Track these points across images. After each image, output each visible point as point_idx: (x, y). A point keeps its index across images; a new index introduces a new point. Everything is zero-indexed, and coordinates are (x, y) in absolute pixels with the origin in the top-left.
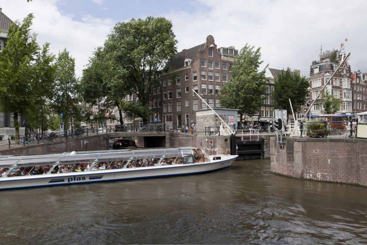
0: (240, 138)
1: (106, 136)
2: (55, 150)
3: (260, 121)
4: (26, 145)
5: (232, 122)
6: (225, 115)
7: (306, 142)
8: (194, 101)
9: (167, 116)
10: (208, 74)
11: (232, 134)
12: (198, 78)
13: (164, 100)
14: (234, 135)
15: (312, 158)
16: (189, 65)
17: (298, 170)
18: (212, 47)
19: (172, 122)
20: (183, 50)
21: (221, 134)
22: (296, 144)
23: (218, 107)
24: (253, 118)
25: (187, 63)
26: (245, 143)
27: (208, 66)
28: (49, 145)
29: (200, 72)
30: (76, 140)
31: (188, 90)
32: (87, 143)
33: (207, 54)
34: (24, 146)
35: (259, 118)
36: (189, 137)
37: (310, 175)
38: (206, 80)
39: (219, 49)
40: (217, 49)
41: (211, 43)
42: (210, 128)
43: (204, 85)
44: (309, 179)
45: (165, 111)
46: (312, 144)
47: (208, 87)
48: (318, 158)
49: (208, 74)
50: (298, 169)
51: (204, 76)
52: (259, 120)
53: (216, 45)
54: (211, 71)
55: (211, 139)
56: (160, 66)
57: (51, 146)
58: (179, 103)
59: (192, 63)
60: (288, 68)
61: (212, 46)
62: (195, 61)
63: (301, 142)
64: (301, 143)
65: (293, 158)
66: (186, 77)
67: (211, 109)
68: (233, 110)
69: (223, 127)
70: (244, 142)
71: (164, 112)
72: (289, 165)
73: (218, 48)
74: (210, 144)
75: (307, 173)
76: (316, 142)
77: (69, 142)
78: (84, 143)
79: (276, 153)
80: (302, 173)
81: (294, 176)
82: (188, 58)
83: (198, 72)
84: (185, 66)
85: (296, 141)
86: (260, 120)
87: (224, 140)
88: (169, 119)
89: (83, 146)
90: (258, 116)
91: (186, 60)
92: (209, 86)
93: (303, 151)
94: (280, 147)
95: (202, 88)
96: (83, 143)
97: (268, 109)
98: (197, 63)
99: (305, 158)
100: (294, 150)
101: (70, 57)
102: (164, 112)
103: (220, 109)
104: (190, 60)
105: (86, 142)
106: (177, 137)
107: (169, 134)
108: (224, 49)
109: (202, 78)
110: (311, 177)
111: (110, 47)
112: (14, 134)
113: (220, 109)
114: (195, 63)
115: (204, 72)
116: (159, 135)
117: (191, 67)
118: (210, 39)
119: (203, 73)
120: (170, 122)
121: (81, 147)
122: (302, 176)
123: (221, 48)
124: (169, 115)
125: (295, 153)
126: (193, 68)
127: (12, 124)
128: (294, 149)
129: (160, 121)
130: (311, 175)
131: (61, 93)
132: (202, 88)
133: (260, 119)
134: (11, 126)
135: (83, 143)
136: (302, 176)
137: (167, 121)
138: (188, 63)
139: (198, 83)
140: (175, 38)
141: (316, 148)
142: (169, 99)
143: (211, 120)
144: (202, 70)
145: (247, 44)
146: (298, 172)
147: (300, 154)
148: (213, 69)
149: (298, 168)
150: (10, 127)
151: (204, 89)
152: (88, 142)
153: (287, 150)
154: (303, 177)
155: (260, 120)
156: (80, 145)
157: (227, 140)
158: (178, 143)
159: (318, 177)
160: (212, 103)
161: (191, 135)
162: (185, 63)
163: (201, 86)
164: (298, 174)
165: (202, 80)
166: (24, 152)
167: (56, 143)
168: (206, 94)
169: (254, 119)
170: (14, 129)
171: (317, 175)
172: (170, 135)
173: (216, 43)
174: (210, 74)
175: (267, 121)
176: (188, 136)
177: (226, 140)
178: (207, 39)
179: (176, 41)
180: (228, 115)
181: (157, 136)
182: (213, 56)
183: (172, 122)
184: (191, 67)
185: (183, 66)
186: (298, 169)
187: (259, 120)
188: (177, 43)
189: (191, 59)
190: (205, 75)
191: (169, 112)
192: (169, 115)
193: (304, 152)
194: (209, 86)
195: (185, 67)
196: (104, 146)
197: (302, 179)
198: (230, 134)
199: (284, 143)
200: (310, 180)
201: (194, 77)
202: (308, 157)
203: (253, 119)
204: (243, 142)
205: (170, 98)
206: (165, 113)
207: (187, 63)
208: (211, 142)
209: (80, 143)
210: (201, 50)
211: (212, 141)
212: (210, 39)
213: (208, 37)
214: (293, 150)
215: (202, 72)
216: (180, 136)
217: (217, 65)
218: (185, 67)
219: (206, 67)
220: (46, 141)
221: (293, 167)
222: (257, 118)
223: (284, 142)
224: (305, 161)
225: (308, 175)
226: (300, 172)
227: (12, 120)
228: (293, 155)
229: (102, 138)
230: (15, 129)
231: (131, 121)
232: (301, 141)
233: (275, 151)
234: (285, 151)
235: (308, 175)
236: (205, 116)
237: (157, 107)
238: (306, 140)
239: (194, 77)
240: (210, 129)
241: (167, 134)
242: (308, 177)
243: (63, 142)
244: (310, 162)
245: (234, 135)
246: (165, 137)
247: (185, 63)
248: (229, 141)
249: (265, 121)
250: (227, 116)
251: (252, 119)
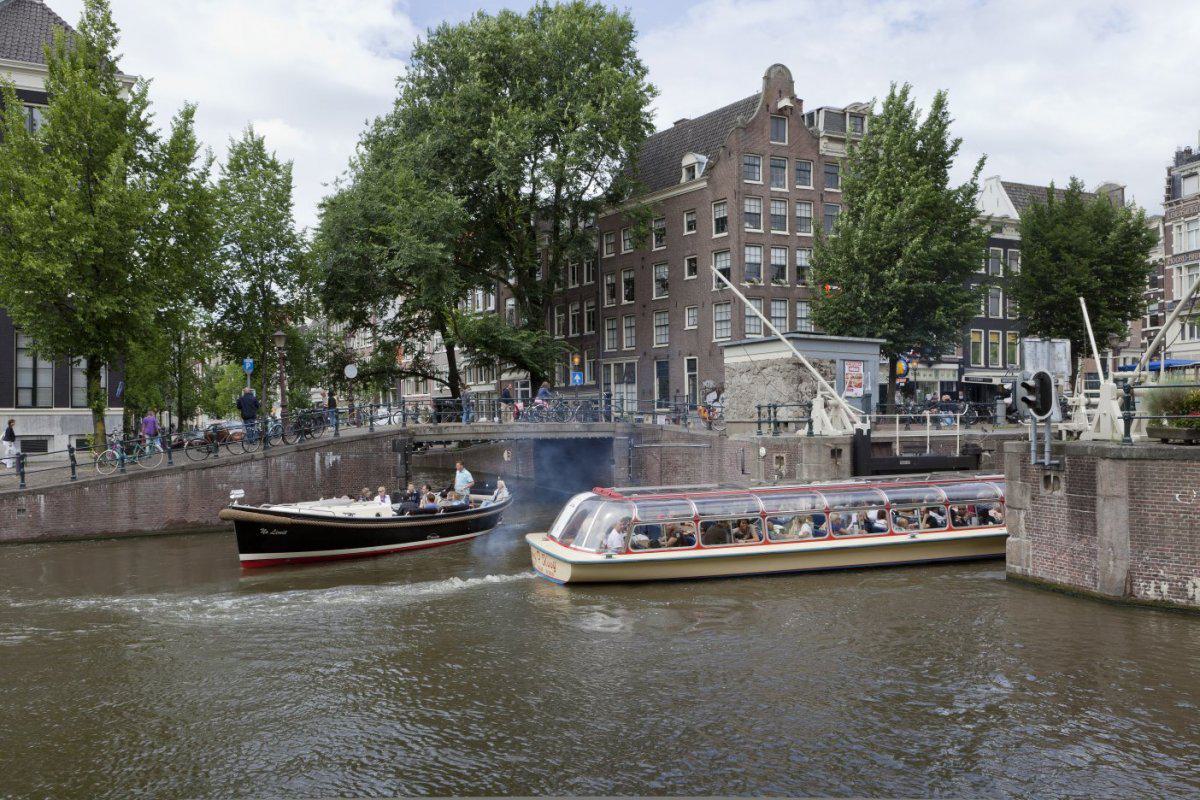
0: (887, 445)
1: (400, 437)
2: (225, 485)
3: (963, 381)
4: (130, 470)
5: (859, 386)
6: (833, 362)
7: (1145, 459)
8: (718, 307)
9: (619, 366)
10: (767, 209)
11: (859, 431)
12: (732, 224)
13: (606, 306)
14: (865, 433)
15: (1169, 522)
16: (698, 175)
17: (1111, 569)
18: (785, 107)
19: (634, 388)
20: (675, 124)
21: (816, 431)
22: (1104, 467)
23: (804, 330)
24: (937, 371)
25: (691, 169)
26: (907, 463)
27: (773, 177)
28: (204, 469)
29: (740, 204)
30: (299, 450)
31: (693, 270)
32: (335, 463)
33: (768, 133)
34: (123, 471)
35: (961, 372)
36: (697, 442)
37: (1159, 588)
38: (761, 231)
39: (811, 116)
40: (803, 116)
41: (780, 92)
42: (775, 407)
43: (753, 249)
44: (1155, 601)
45: (608, 346)
46: (1170, 467)
47: (793, 259)
48: (1192, 522)
49: (767, 209)
50: (1111, 563)
51: (754, 218)
52: (960, 378)
53: (800, 102)
54: (780, 198)
55: (778, 448)
56: (594, 182)
57: (212, 471)
58: (663, 316)
59: (710, 168)
60: (1073, 179)
61: (785, 102)
62: (722, 163)
63: (1125, 459)
64: (1125, 465)
65: (1094, 521)
66: (689, 223)
67: (779, 340)
68: (855, 342)
69: (826, 406)
70: (905, 459)
71: (607, 350)
72: (1078, 546)
73: (806, 109)
74: (776, 466)
75: (1148, 579)
76: (1185, 460)
77: (273, 460)
78: (327, 463)
79: (1027, 500)
80: (1130, 580)
81: (1097, 590)
82: (696, 152)
83: (731, 200)
84: (684, 180)
85: (1105, 458)
86: (963, 378)
87: (829, 452)
88: (627, 376)
89: (323, 474)
90: (959, 362)
91: (689, 159)
92: (773, 252)
93: (1132, 494)
94: (1041, 479)
95: (747, 260)
96: (322, 462)
97: (978, 335)
98: (728, 169)
99: (1142, 522)
100: (1100, 491)
101: (270, 157)
102: (607, 350)
103: (812, 336)
104: (704, 159)
105: (331, 458)
106: (656, 441)
107: (626, 431)
108: (829, 113)
109: (747, 225)
110: (1165, 593)
111: (414, 121)
112: (88, 430)
113: (812, 336)
114: (720, 171)
115: (753, 202)
116: (590, 435)
117: (704, 184)
118: (779, 79)
119: (751, 206)
120: (629, 387)
121: (313, 475)
122: (1128, 591)
123: (818, 110)
124: (625, 361)
125: (1100, 502)
126: (715, 190)
127: (80, 396)
128: (1099, 486)
129: (593, 383)
130: (1165, 587)
131: (243, 287)
132: (747, 260)
133: (967, 375)
134: (21, 402)
135: (322, 462)
136: (1128, 591)
137: (619, 382)
138: (696, 169)
139: (732, 244)
140: (647, 80)
141: (1185, 483)
142: (625, 302)
143: (780, 380)
144: (748, 193)
145: (894, 87)
146: (1114, 575)
147: (1123, 507)
148: (786, 190)
149: (1114, 560)
150: (16, 407)
151: (755, 264)
152: (339, 457)
153: (1068, 491)
154: (1131, 594)
155: (967, 379)
156: (313, 468)
157: (840, 451)
158: (658, 465)
159: (1190, 594)
160: (783, 315)
161: (705, 433)
162: (684, 170)
163: (742, 256)
164: (1112, 580)
165: (747, 230)
166: (122, 492)
167: (228, 464)
168: (762, 284)
169: (940, 373)
170: (89, 412)
171: (1189, 586)
172: (630, 435)
173: (799, 92)
174: (778, 209)
175: (991, 380)
176: (692, 438)
177: (836, 453)
178: (767, 78)
179: (650, 88)
180: (844, 360)
181: (582, 436)
182: (787, 143)
183: (634, 388)
184: (704, 184)
185: (674, 182)
186: (1111, 563)
187: (960, 378)
188: (654, 95)
189: (705, 153)
190: (760, 215)
191: (625, 349)
192: (625, 361)
193: (1135, 497)
194: (773, 252)
195: (685, 185)
196: (395, 475)
197: (1126, 604)
198: (851, 430)
199: (1058, 465)
200: (1163, 608)
201: (717, 220)
202: (1152, 518)
203: (937, 375)
204: (898, 459)
205: (628, 298)
206: (611, 355)
207: (691, 169)
208: (780, 459)
209: (313, 461)
210: (742, 120)
211: (784, 455)
212: (779, 79)
213: (769, 70)
214: (1094, 491)
215: (747, 202)
216: (666, 436)
217: (801, 173)
218: (686, 185)
219: (761, 182)
220: (197, 456)
221: (1093, 554)
222: (954, 370)
223: (1057, 462)
224: (1139, 531)
225: (1153, 585)
226: (1121, 575)
227: (80, 380)
228: (1094, 510)
229: (388, 445)
230: (91, 413)
231: (488, 383)
232: (1124, 456)
233: (1024, 493)
234: (1060, 493)
235: (1153, 585)
236: (759, 365)
237: (581, 331)
238: (1145, 454)
239: (717, 220)
240: (775, 413)
241: (619, 431)
242: (1152, 594)
243: (253, 459)
244: (1162, 534)
245: (865, 433)
246: (610, 440)
247: (684, 170)
248: (846, 457)
249: (984, 380)
250: (839, 364)
251: (933, 373)
